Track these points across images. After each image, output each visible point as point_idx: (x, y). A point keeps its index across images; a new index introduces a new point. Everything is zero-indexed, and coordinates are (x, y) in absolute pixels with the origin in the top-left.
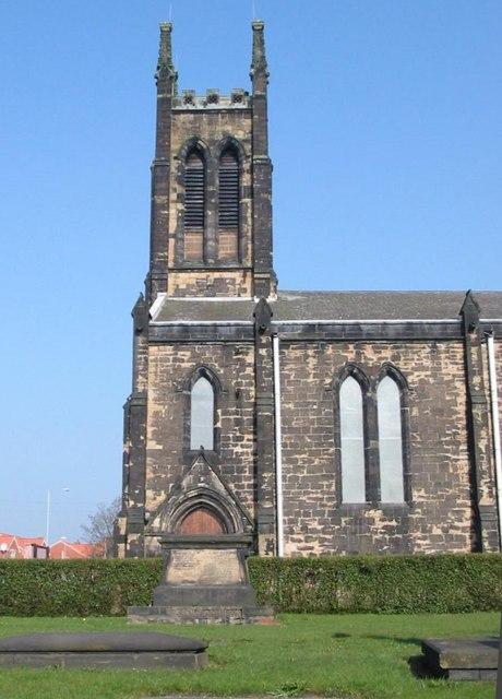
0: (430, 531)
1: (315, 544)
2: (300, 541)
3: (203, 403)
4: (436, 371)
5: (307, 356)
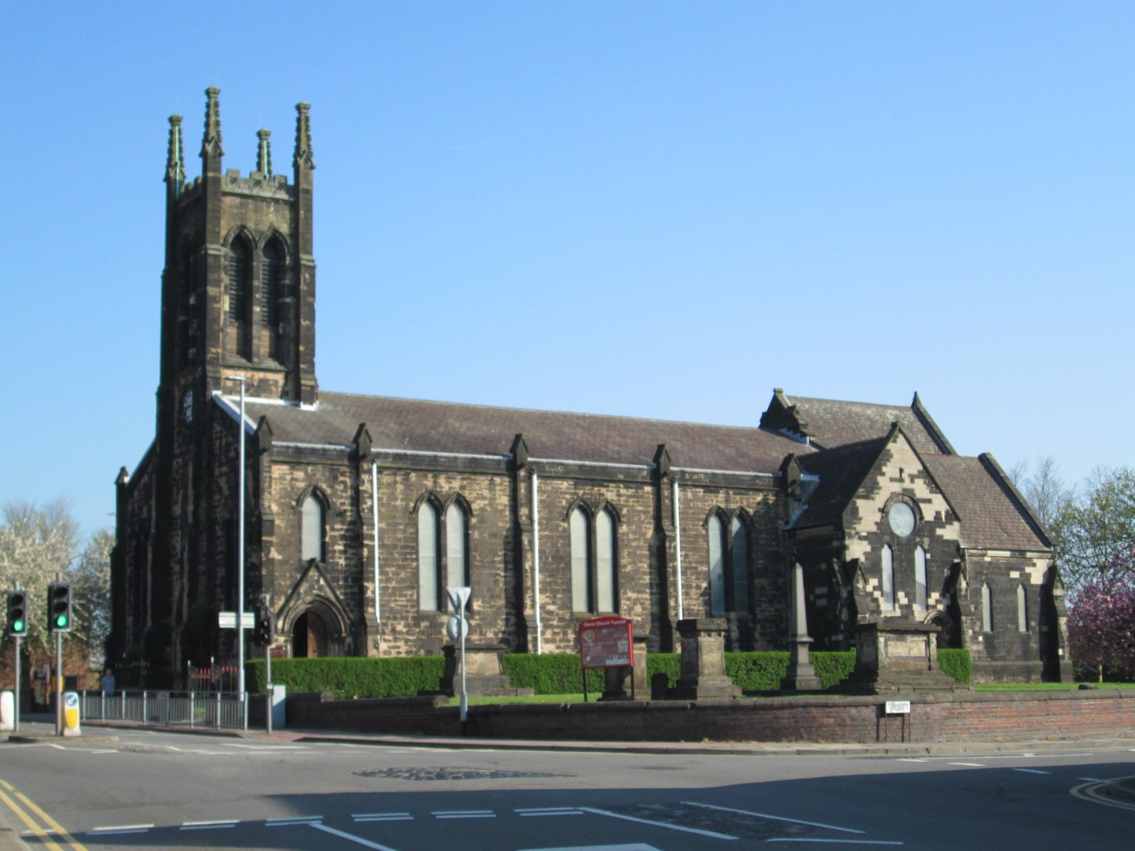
0: (485, 634)
1: (401, 644)
2: (389, 641)
3: (454, 556)
4: (492, 499)
5: (396, 482)
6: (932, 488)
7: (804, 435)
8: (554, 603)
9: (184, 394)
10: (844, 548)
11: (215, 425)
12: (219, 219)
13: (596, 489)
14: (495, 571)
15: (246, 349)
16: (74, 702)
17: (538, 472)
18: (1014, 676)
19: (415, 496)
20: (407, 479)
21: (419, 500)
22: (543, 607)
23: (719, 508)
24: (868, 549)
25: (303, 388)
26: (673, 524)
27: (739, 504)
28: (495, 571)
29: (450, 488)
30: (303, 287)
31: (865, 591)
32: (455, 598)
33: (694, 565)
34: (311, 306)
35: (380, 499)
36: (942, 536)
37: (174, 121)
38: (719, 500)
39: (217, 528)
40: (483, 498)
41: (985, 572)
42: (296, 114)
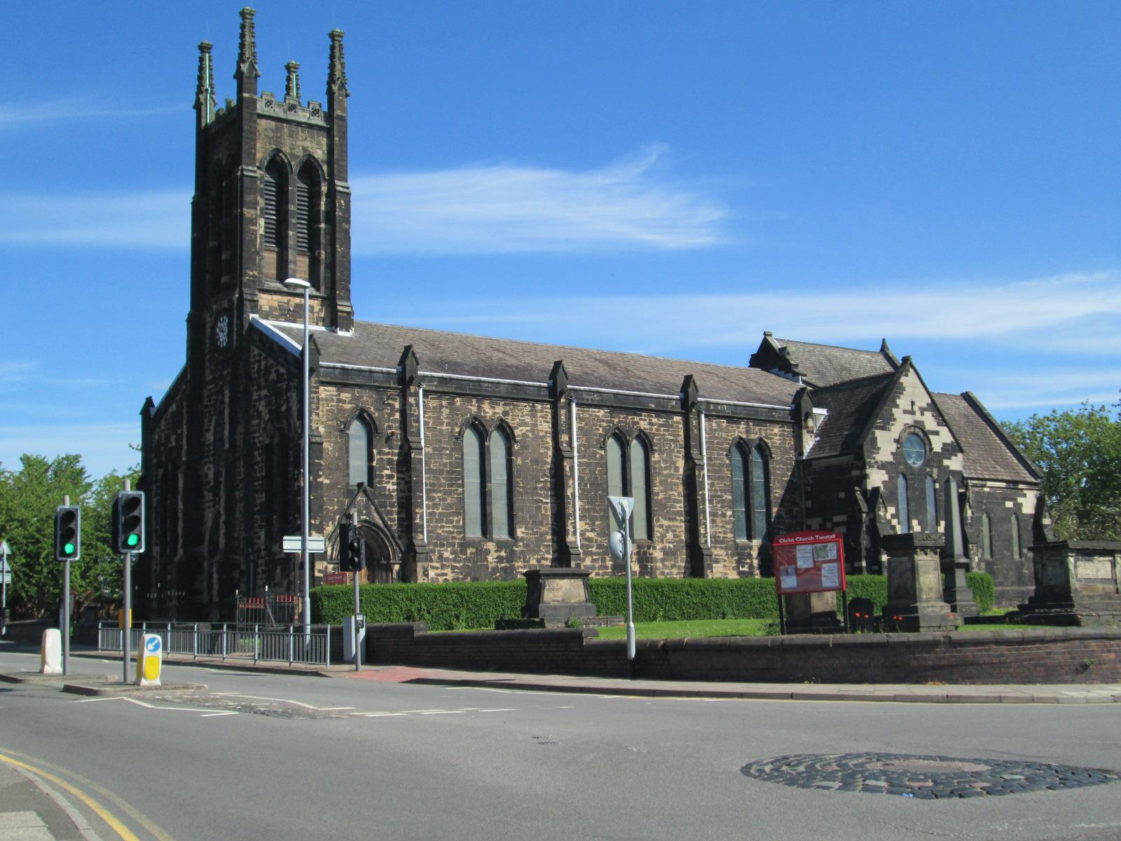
0: (528, 561)
1: (448, 571)
2: (437, 568)
5: (441, 407)
6: (939, 420)
7: (796, 374)
8: (593, 530)
9: (217, 320)
10: (866, 477)
11: (253, 348)
12: (254, 140)
13: (630, 417)
14: (536, 498)
15: (282, 273)
16: (156, 647)
17: (577, 399)
18: (1011, 600)
19: (460, 420)
20: (452, 404)
21: (463, 426)
22: (582, 534)
23: (741, 438)
24: (886, 478)
25: (339, 314)
26: (701, 453)
27: (758, 435)
28: (536, 498)
29: (494, 413)
30: (338, 213)
31: (886, 519)
32: (619, 510)
33: (719, 493)
34: (347, 232)
35: (426, 423)
36: (948, 467)
37: (203, 48)
38: (740, 430)
39: (256, 453)
40: (526, 424)
41: (985, 501)
42: (329, 42)
